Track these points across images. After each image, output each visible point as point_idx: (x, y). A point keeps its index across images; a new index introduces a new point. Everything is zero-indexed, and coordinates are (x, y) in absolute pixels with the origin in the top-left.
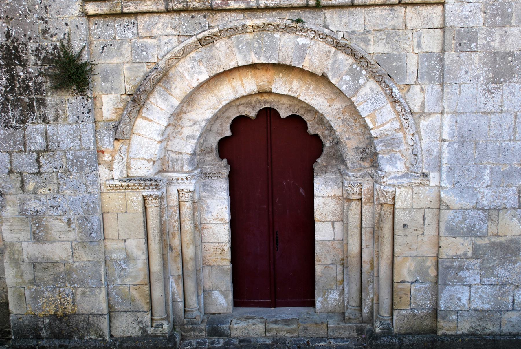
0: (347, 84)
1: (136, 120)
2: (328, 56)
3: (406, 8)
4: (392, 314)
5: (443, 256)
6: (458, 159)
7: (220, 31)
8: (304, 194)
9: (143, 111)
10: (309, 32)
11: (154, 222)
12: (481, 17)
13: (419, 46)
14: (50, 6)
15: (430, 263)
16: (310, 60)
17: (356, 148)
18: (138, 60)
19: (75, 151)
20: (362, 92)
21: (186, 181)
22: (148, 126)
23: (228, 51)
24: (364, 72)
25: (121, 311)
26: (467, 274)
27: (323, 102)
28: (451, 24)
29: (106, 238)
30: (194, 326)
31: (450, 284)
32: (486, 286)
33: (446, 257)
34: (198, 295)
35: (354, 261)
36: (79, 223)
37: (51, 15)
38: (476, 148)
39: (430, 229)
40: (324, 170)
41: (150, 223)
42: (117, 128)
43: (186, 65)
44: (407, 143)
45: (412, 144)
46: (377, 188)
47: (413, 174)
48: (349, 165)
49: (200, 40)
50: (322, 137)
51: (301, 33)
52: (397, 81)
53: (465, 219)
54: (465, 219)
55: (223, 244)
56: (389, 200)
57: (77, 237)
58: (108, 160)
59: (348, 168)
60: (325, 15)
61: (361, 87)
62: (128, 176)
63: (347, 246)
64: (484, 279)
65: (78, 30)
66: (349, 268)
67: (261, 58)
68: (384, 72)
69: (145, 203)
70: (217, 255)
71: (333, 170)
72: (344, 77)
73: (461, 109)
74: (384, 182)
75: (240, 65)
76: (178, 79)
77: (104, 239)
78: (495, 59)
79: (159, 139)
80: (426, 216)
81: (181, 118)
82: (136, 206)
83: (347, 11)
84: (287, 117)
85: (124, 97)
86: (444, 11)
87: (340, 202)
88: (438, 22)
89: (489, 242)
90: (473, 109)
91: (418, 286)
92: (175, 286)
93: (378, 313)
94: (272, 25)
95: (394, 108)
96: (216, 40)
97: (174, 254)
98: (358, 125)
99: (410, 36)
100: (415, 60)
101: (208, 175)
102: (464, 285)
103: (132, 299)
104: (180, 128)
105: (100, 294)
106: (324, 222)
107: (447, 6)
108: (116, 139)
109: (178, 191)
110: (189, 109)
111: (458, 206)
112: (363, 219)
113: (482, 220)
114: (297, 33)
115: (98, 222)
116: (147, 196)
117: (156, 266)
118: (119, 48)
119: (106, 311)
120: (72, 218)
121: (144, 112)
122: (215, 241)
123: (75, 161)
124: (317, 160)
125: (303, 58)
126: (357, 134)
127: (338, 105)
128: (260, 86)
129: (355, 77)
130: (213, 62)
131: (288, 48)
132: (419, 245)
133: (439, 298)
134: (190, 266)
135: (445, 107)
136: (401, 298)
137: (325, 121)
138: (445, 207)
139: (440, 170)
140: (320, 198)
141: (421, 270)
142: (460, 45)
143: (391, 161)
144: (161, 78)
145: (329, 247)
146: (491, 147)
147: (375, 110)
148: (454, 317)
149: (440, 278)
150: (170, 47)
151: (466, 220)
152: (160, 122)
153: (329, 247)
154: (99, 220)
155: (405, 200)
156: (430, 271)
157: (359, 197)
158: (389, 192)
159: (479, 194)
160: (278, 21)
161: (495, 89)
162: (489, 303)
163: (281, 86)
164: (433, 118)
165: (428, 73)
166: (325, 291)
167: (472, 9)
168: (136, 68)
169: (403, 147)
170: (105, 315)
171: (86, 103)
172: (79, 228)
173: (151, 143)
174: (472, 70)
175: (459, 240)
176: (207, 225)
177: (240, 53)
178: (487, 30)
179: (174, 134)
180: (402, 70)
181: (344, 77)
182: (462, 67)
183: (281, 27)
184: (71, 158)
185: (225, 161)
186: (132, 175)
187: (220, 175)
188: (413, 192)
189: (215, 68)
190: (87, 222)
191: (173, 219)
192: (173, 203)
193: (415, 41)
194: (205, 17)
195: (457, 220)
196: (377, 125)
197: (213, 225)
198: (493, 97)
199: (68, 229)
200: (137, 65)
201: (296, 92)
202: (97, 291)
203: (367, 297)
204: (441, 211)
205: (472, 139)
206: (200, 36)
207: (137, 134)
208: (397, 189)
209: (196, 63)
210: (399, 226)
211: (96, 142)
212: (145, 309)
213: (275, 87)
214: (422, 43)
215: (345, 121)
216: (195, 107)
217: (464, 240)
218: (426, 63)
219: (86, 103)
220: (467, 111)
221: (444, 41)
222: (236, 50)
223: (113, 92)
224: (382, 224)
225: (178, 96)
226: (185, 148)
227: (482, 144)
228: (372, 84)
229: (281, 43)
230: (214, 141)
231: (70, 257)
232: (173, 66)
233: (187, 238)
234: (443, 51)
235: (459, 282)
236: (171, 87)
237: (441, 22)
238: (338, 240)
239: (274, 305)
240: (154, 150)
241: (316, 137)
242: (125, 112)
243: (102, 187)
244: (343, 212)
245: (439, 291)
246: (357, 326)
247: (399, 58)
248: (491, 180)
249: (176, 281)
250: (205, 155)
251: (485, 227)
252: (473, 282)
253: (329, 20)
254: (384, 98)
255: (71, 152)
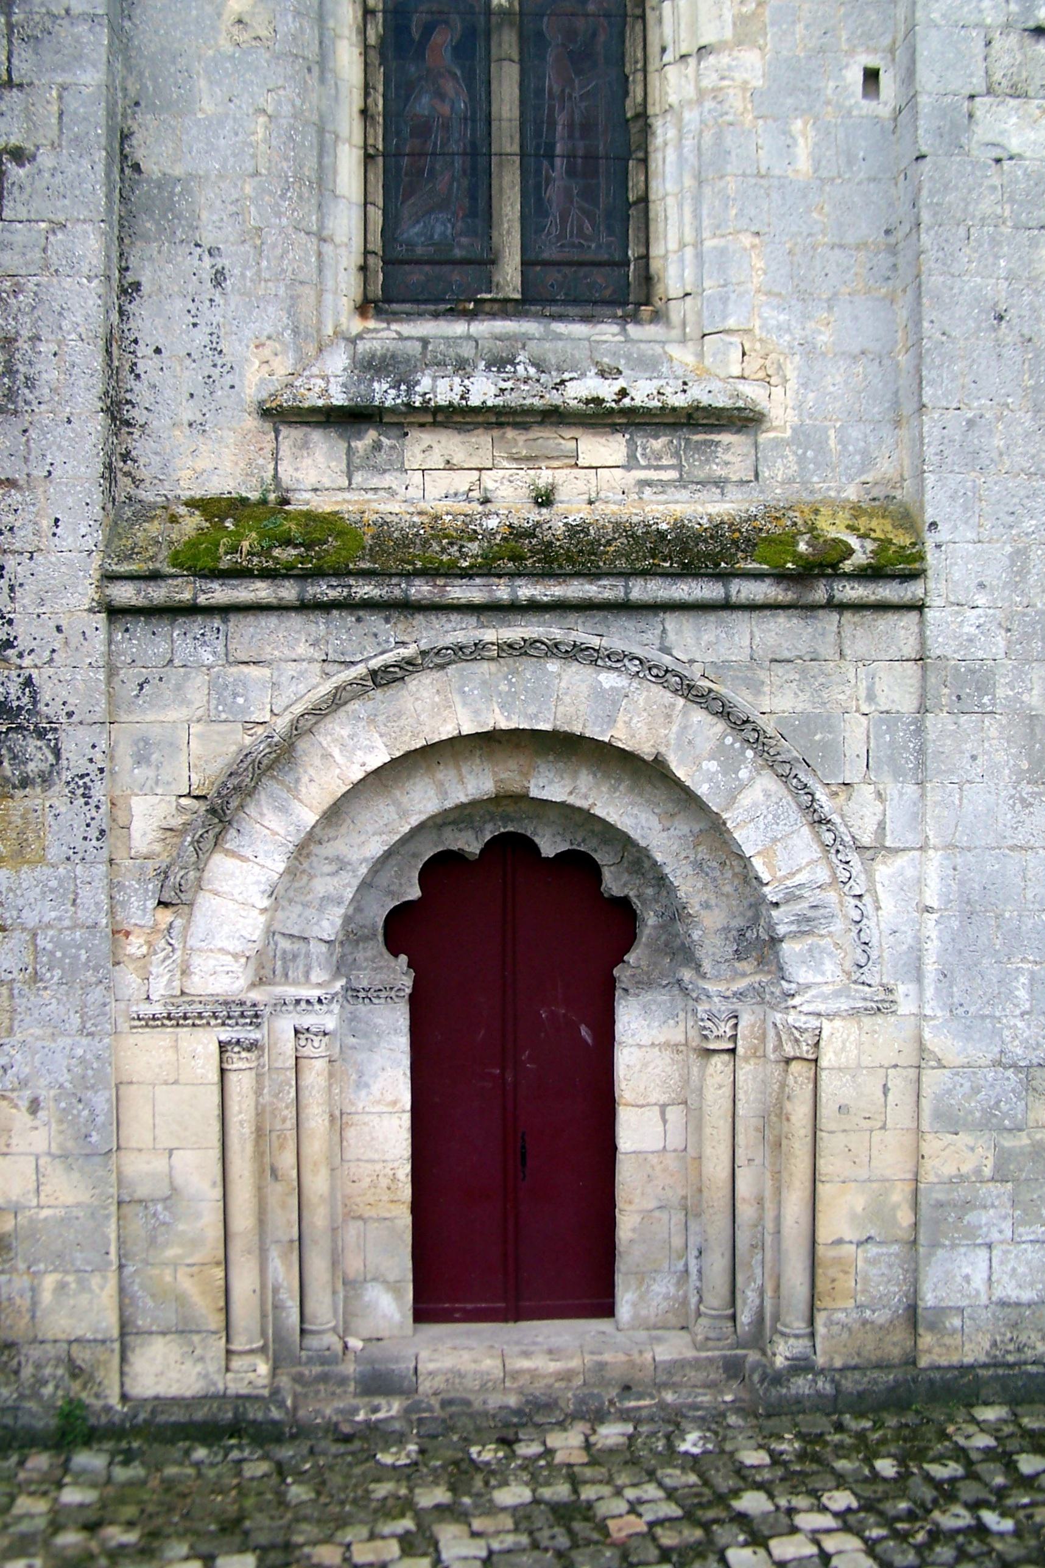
0: (711, 780)
1: (208, 859)
2: (669, 716)
3: (841, 614)
4: (811, 1322)
5: (929, 1177)
6: (960, 952)
7: (424, 653)
8: (589, 1041)
9: (228, 837)
10: (626, 661)
11: (244, 1106)
12: (1000, 641)
13: (871, 697)
14: (21, 585)
15: (899, 1195)
16: (627, 723)
17: (724, 929)
18: (223, 716)
19: (60, 931)
20: (746, 799)
21: (317, 1007)
22: (237, 873)
23: (437, 699)
24: (750, 754)
25: (151, 1333)
26: (984, 1217)
27: (647, 820)
28: (938, 652)
29: (123, 1144)
30: (326, 1368)
31: (947, 1243)
32: (1024, 1246)
33: (935, 1180)
34: (334, 1292)
35: (718, 1196)
36: (58, 1108)
37: (24, 606)
38: (998, 927)
39: (900, 1114)
40: (645, 983)
41: (233, 1107)
42: (167, 877)
43: (338, 729)
44: (846, 916)
45: (858, 919)
46: (778, 1022)
47: (861, 987)
48: (707, 966)
49: (373, 673)
50: (637, 904)
51: (609, 663)
52: (824, 775)
53: (976, 1090)
54: (976, 1090)
55: (396, 1165)
56: (805, 1048)
57: (53, 1145)
58: (139, 953)
59: (704, 976)
60: (663, 622)
61: (742, 787)
62: (183, 993)
63: (700, 1165)
64: (1021, 1230)
65: (85, 643)
66: (705, 1217)
67: (515, 718)
68: (795, 754)
69: (221, 1062)
70: (379, 1191)
71: (664, 983)
72: (706, 765)
73: (964, 841)
74: (794, 1007)
75: (464, 733)
76: (317, 761)
77: (118, 1148)
78: (1032, 730)
79: (266, 903)
80: (889, 1085)
81: (308, 856)
82: (203, 1067)
83: (712, 617)
84: (557, 855)
85: (184, 801)
86: (922, 622)
87: (680, 1057)
88: (910, 649)
89: (1028, 1142)
90: (990, 840)
91: (873, 1250)
92: (282, 1271)
93: (776, 1318)
94: (543, 643)
95: (818, 835)
96: (412, 672)
97: (279, 1188)
98: (729, 874)
99: (851, 675)
100: (863, 730)
101: (362, 994)
102: (976, 1245)
103: (181, 1299)
104: (305, 878)
105: (102, 1288)
106: (642, 1106)
107: (929, 614)
108: (160, 903)
109: (296, 1032)
110: (331, 833)
111: (962, 1060)
112: (740, 1095)
113: (1013, 1091)
114: (600, 662)
115: (106, 1107)
116: (229, 1043)
117: (243, 1221)
118: (179, 688)
119: (115, 1333)
120: (43, 1094)
121: (232, 840)
122: (376, 1157)
123: (59, 954)
124: (626, 958)
125: (612, 720)
126: (728, 896)
127: (683, 827)
128: (501, 781)
129: (730, 766)
130: (402, 722)
131: (577, 696)
132: (874, 1153)
133: (921, 1277)
134: (319, 1219)
135: (931, 834)
136: (833, 1280)
137: (647, 865)
138: (933, 1063)
139: (919, 979)
140: (633, 1049)
141: (879, 1211)
142: (959, 697)
143: (812, 956)
144: (276, 760)
145: (653, 1167)
146: (1030, 926)
147: (775, 840)
148: (957, 1322)
149: (922, 1230)
150: (302, 688)
151: (979, 1092)
152: (269, 863)
153: (653, 1167)
154: (108, 1100)
155: (843, 1049)
156: (899, 1214)
157: (731, 1046)
158: (806, 1030)
159: (1006, 1032)
160: (557, 633)
161: (1032, 794)
162: (1032, 1284)
163: (551, 782)
164: (902, 860)
165: (891, 759)
166: (642, 1277)
167: (982, 620)
168: (219, 733)
169: (838, 926)
170: (112, 1341)
171: (94, 814)
172: (61, 1121)
173: (244, 913)
174: (985, 753)
175: (965, 1139)
176: (356, 1117)
177: (465, 704)
178: (1015, 667)
179: (291, 894)
180: (832, 751)
181: (706, 765)
182: (964, 747)
183: (563, 648)
184: (49, 946)
185: (403, 958)
186: (192, 991)
187: (393, 994)
188: (860, 1028)
189: (407, 738)
190: (80, 1107)
191: (282, 1100)
192: (284, 1062)
193: (863, 686)
194: (387, 621)
195: (959, 1092)
196: (779, 874)
197: (371, 1117)
198: (1031, 813)
199: (30, 1124)
200: (223, 727)
201: (586, 797)
202: (95, 1281)
203: (749, 1285)
204: (924, 1072)
205: (990, 907)
206: (375, 664)
207: (210, 891)
208: (825, 1021)
209: (361, 724)
210: (827, 1110)
211: (112, 912)
212: (213, 1327)
213: (537, 786)
214: (878, 692)
215: (699, 865)
216: (343, 830)
217: (976, 1139)
218: (888, 738)
219: (94, 814)
220: (977, 843)
221: (924, 688)
222: (457, 698)
223: (159, 791)
224: (788, 1106)
225: (315, 803)
226: (316, 928)
227: (1011, 918)
228: (767, 782)
229: (563, 684)
230: (378, 913)
231: (32, 1196)
232: (305, 732)
233: (316, 1146)
234: (923, 709)
235: (965, 1237)
236: (298, 780)
237: (918, 648)
238: (675, 1151)
239: (515, 1314)
240: (250, 929)
241: (625, 901)
242: (189, 839)
243: (120, 1020)
244: (687, 1081)
245: (922, 1262)
246: (724, 1357)
247: (826, 723)
248: (1032, 999)
249: (284, 1256)
250: (357, 944)
251: (1021, 1105)
252: (995, 1236)
253: (672, 637)
254: (794, 814)
255: (51, 933)
